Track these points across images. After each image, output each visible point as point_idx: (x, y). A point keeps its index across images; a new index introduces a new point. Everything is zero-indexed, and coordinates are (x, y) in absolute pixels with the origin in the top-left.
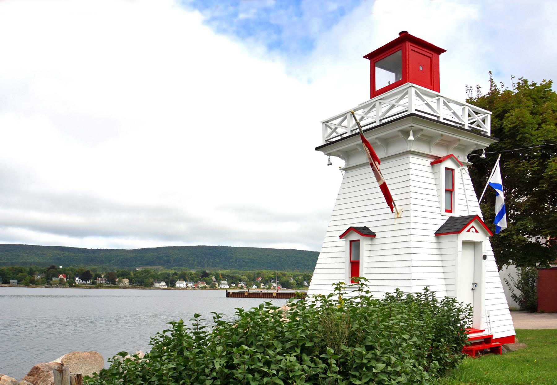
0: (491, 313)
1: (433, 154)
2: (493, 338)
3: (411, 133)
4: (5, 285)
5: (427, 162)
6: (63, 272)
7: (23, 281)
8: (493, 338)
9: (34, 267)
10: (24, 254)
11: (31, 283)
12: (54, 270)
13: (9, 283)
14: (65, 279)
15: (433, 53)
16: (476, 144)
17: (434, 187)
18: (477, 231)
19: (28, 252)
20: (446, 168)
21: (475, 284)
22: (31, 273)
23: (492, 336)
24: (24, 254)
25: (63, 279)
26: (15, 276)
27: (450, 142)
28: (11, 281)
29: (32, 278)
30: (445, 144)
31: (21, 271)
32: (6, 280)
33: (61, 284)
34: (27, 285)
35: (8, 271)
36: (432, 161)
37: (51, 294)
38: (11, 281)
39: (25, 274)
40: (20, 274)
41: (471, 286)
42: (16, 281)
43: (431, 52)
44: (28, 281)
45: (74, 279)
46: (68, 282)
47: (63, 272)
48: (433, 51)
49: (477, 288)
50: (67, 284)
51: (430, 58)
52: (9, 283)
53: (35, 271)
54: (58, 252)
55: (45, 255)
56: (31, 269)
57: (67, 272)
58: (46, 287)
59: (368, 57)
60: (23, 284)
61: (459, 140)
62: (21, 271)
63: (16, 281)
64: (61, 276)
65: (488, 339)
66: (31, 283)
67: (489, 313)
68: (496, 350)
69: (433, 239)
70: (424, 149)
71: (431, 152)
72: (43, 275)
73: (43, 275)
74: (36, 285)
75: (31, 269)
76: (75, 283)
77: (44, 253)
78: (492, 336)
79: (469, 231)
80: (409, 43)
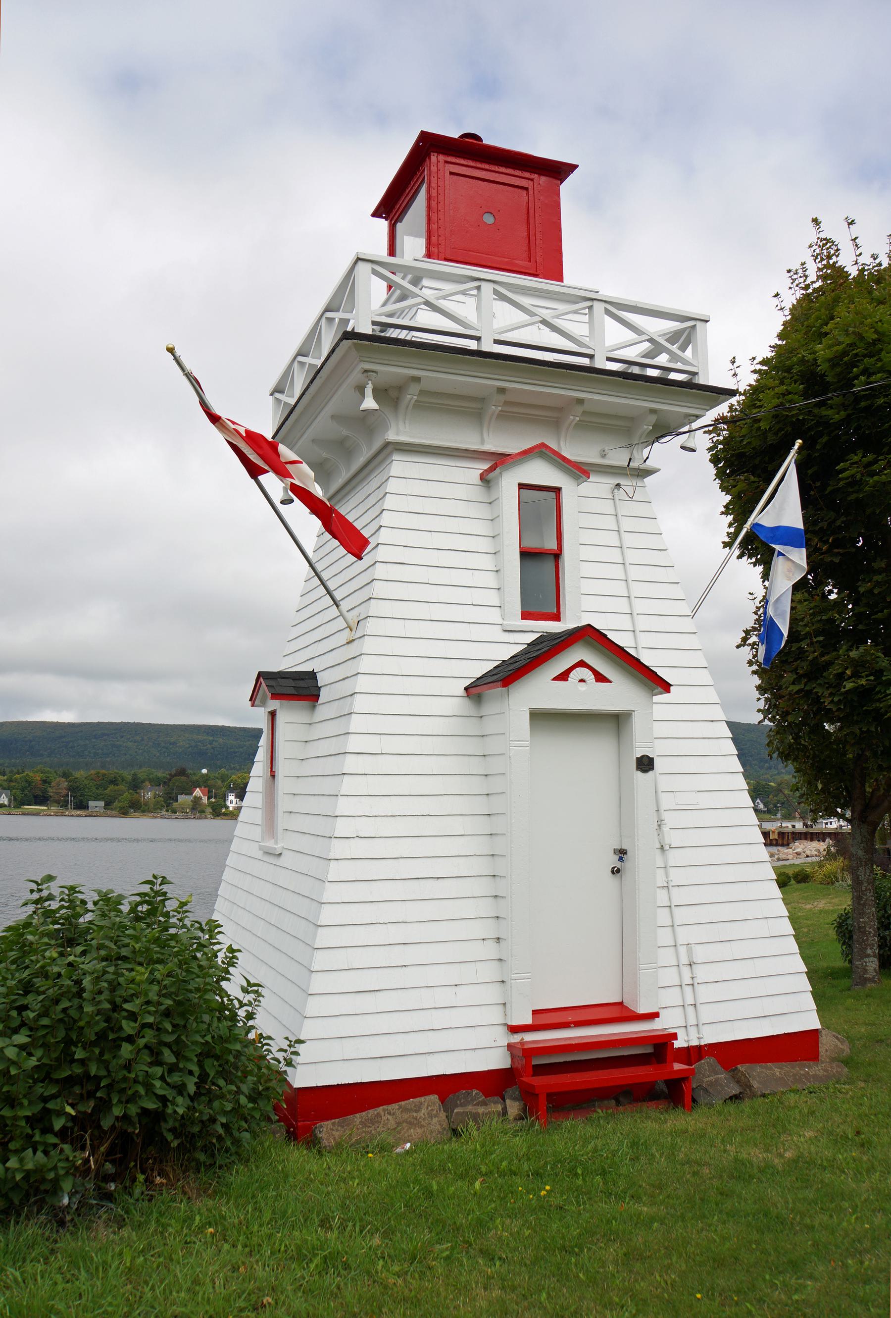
0: (700, 954)
1: (489, 447)
2: (677, 1044)
3: (369, 390)
4: (78, 812)
5: (474, 470)
6: (204, 782)
7: (116, 804)
8: (677, 1044)
9: (142, 773)
10: (130, 744)
11: (131, 807)
12: (183, 778)
13: (86, 807)
14: (205, 800)
15: (535, 176)
16: (653, 411)
17: (484, 545)
18: (600, 678)
19: (138, 738)
20: (521, 486)
21: (622, 853)
22: (136, 785)
23: (674, 1036)
24: (130, 744)
25: (200, 798)
26: (98, 792)
27: (560, 409)
28: (91, 803)
29: (136, 796)
30: (516, 413)
31: (114, 782)
32: (81, 801)
33: (196, 809)
34: (124, 813)
35: (86, 782)
36: (486, 466)
37: (74, 836)
38: (91, 803)
39: (122, 787)
40: (112, 787)
41: (612, 860)
42: (102, 804)
43: (527, 175)
44: (126, 803)
45: (225, 798)
46: (211, 805)
47: (204, 782)
48: (531, 172)
49: (627, 866)
50: (209, 810)
51: (526, 189)
52: (86, 807)
53: (143, 782)
54: (200, 738)
55: (174, 744)
56: (135, 778)
57: (210, 782)
58: (163, 817)
59: (376, 214)
60: (115, 809)
61: (580, 401)
62: (114, 782)
63: (102, 804)
64: (198, 792)
65: (662, 1044)
66: (134, 807)
67: (690, 953)
68: (676, 1093)
69: (457, 704)
70: (468, 439)
71: (483, 442)
72: (160, 791)
73: (160, 791)
74: (143, 812)
75: (135, 778)
76: (227, 807)
77: (172, 740)
78: (674, 1036)
79: (563, 676)
80: (442, 158)
